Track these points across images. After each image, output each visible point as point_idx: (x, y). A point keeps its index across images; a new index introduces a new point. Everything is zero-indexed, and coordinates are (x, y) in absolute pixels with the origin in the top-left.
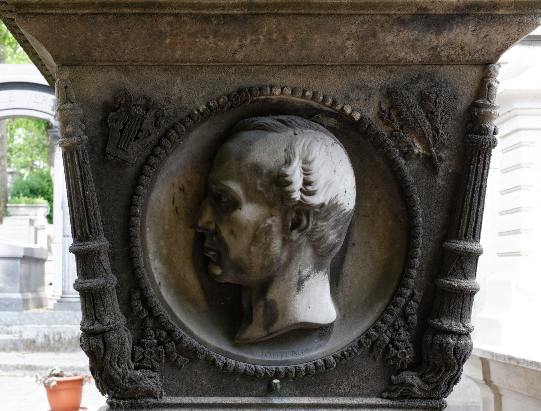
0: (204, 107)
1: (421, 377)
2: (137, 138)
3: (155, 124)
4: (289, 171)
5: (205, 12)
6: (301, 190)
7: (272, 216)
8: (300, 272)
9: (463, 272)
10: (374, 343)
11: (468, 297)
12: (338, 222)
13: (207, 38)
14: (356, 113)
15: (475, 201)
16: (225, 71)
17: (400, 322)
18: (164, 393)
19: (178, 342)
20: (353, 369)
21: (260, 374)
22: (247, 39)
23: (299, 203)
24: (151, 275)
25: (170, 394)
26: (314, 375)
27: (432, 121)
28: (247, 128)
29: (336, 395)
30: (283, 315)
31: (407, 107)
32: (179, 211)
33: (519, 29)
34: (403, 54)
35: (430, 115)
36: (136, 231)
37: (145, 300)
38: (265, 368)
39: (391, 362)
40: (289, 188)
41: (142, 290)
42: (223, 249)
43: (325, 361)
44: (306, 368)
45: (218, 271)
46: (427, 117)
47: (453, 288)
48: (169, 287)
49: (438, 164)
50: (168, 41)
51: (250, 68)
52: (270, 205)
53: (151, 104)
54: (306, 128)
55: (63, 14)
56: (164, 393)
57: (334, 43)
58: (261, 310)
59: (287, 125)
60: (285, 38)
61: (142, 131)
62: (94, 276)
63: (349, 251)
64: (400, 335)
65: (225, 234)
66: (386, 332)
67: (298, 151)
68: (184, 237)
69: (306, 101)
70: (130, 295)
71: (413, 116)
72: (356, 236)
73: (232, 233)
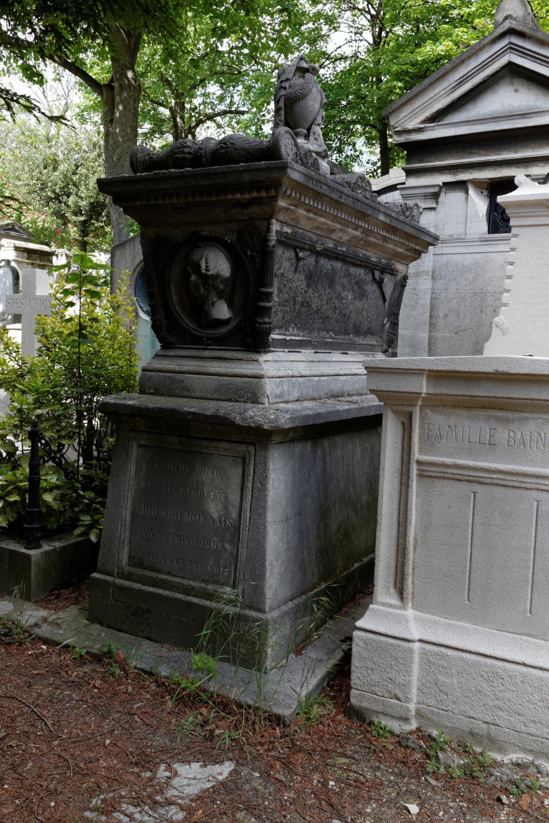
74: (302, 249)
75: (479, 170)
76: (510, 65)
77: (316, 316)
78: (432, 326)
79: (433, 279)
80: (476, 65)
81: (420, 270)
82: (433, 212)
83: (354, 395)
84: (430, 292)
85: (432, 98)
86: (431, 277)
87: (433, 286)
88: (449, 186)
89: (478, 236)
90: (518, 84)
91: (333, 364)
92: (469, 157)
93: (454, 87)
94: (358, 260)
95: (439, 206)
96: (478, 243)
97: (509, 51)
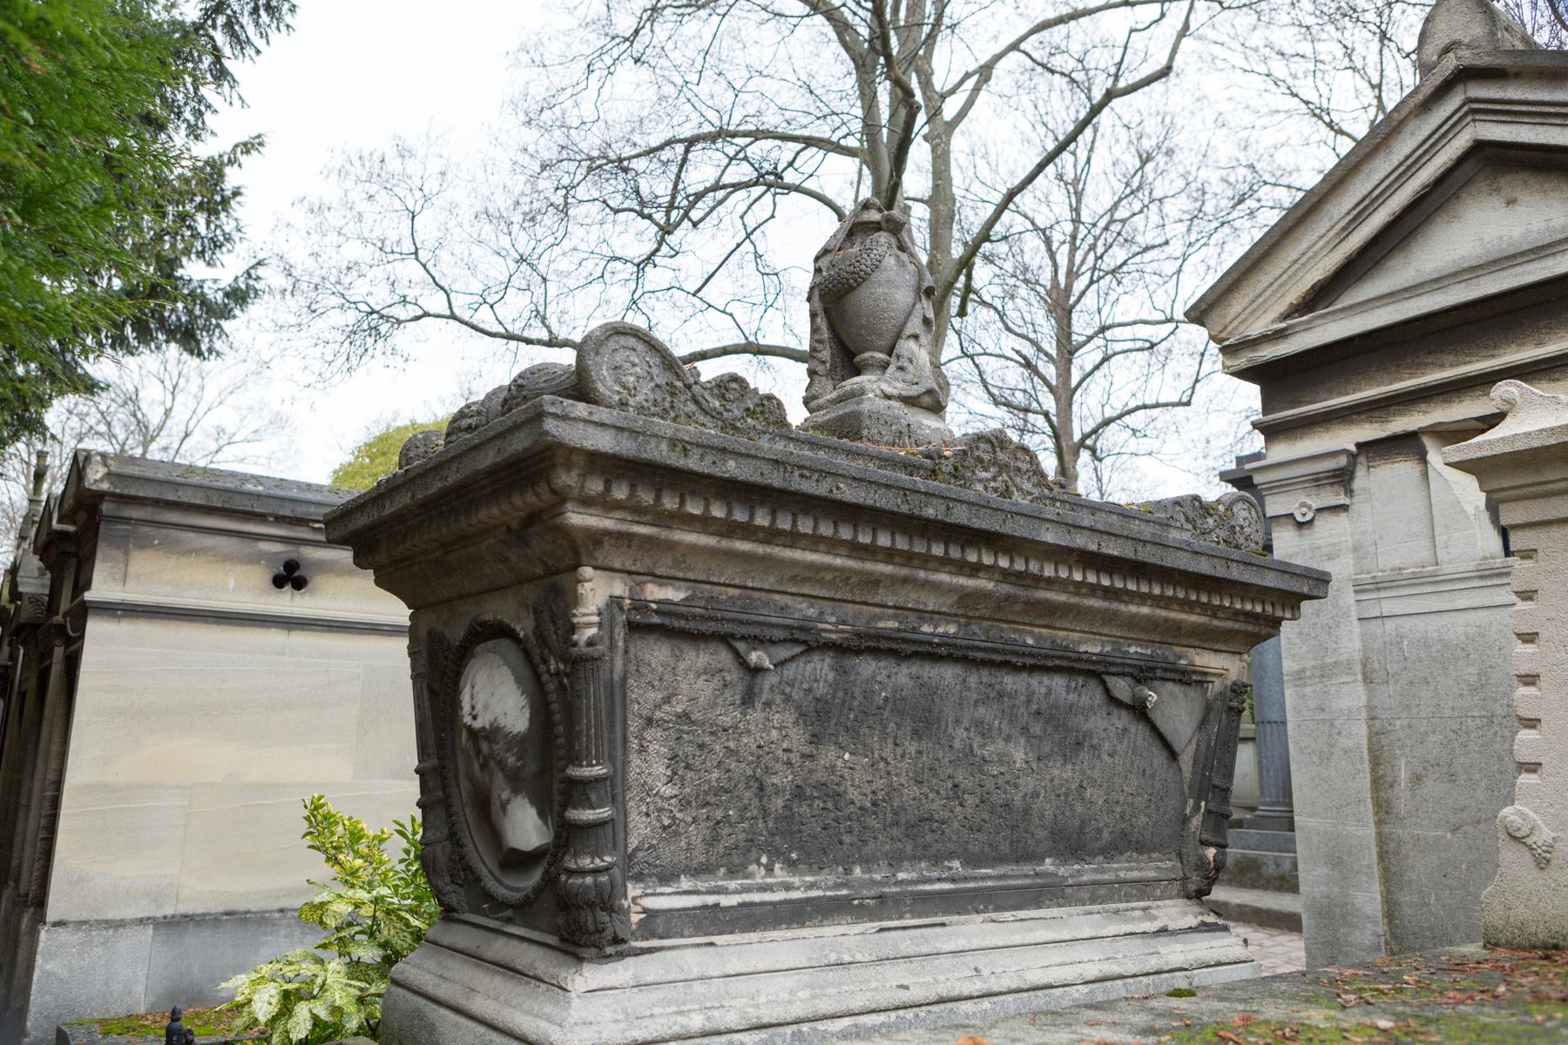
74: (758, 641)
75: (1444, 401)
76: (1481, 151)
77: (871, 821)
78: (1383, 809)
79: (1368, 680)
80: (1389, 169)
81: (1328, 660)
82: (1343, 516)
84: (1364, 715)
85: (1295, 262)
86: (1360, 677)
87: (1369, 700)
88: (1374, 450)
89: (1472, 565)
90: (1511, 184)
91: (946, 961)
92: (1412, 376)
93: (1344, 229)
94: (1016, 653)
95: (1355, 499)
96: (1476, 583)
97: (1469, 118)
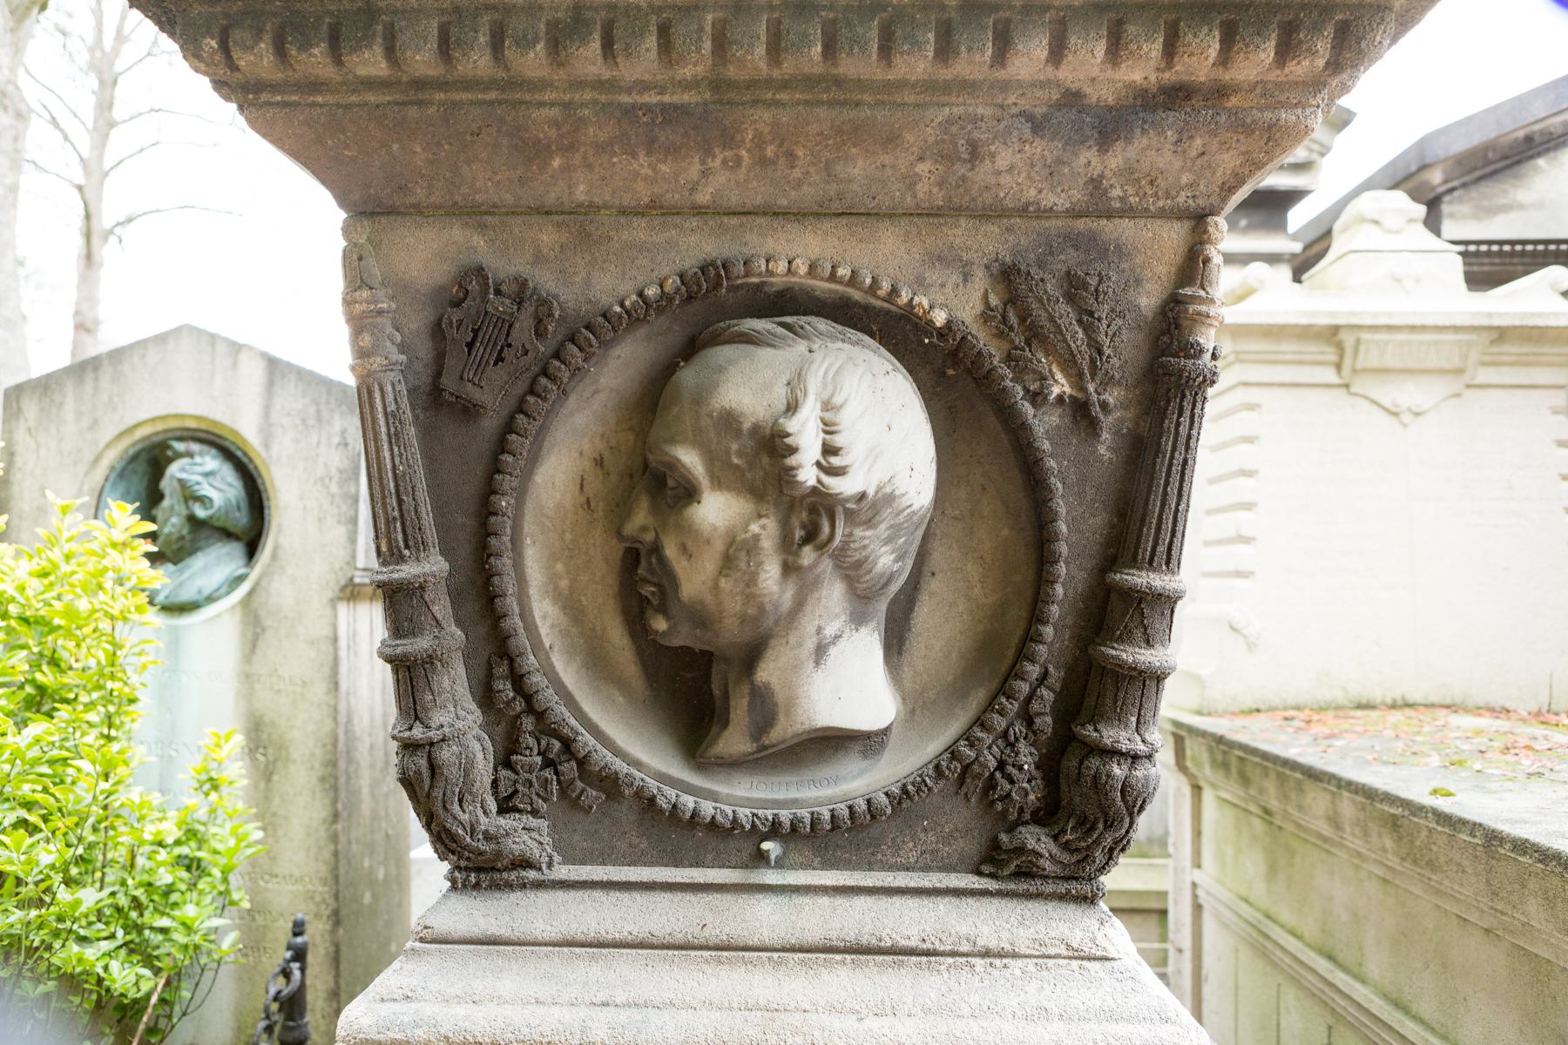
0: (634, 297)
1: (1055, 838)
2: (500, 359)
3: (536, 333)
4: (792, 425)
5: (626, 99)
6: (818, 464)
7: (760, 516)
8: (819, 630)
9: (1145, 633)
10: (966, 768)
11: (1153, 684)
12: (896, 530)
13: (634, 155)
14: (937, 311)
15: (1173, 491)
16: (675, 227)
17: (1019, 728)
18: (557, 858)
19: (583, 763)
20: (924, 818)
21: (743, 827)
22: (714, 156)
23: (814, 490)
24: (531, 628)
25: (568, 860)
26: (849, 830)
27: (1089, 329)
28: (717, 340)
29: (891, 868)
30: (788, 713)
31: (1040, 301)
32: (593, 505)
33: (1269, 139)
34: (1033, 192)
35: (1087, 319)
36: (503, 542)
37: (518, 680)
38: (754, 815)
39: (999, 806)
40: (792, 461)
41: (512, 661)
42: (667, 581)
43: (869, 801)
44: (833, 816)
45: (660, 624)
46: (1080, 322)
47: (1122, 665)
48: (570, 651)
49: (1101, 416)
50: (556, 162)
51: (725, 219)
52: (756, 494)
53: (528, 293)
54: (833, 338)
55: (338, 105)
56: (557, 858)
57: (893, 167)
58: (744, 702)
59: (795, 333)
60: (791, 156)
61: (509, 346)
62: (412, 633)
63: (924, 586)
64: (1017, 754)
65: (670, 551)
66: (990, 748)
67: (814, 384)
68: (603, 556)
69: (840, 288)
70: (490, 667)
71: (1052, 319)
72: (940, 556)
73: (684, 549)
83: (335, 626)
